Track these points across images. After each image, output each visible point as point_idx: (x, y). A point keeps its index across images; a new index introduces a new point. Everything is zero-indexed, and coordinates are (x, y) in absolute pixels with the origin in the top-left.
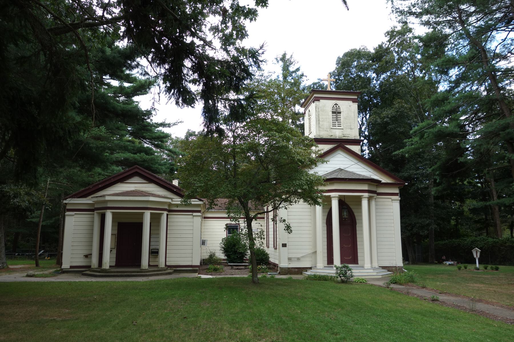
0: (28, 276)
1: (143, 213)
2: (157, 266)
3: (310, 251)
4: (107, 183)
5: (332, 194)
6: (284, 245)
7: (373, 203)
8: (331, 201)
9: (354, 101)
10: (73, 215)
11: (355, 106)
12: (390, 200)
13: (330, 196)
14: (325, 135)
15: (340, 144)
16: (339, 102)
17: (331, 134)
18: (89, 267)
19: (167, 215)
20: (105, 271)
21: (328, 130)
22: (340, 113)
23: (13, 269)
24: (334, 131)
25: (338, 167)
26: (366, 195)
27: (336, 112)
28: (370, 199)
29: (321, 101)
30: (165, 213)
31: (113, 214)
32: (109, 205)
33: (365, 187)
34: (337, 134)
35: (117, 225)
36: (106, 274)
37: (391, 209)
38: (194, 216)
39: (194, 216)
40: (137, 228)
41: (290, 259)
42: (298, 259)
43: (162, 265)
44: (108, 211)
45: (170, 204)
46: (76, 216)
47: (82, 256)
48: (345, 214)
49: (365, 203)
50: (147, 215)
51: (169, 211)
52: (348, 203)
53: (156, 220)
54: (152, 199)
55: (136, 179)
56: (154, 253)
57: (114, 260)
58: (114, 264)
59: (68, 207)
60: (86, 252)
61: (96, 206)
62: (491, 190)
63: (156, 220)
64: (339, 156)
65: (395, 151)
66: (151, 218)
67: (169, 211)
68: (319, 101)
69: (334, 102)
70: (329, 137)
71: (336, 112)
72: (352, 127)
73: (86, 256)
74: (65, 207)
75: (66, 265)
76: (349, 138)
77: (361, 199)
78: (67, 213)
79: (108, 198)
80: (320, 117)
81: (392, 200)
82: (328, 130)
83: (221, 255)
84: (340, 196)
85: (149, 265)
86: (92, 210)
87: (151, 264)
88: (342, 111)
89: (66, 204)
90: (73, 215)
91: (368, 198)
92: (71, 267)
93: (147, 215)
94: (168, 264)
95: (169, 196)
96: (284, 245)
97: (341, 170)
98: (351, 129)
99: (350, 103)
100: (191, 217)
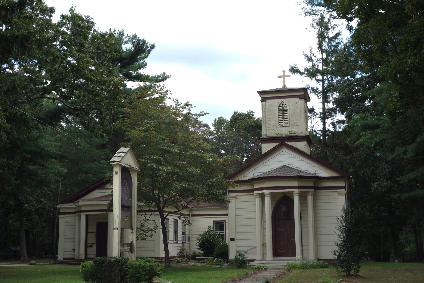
0: (31, 264)
5: (264, 192)
12: (336, 194)
13: (263, 193)
16: (284, 100)
17: (277, 132)
21: (275, 129)
22: (286, 110)
23: (225, 268)
24: (281, 129)
25: (283, 164)
27: (283, 111)
32: (83, 209)
33: (295, 183)
34: (284, 131)
35: (96, 224)
37: (335, 204)
44: (82, 213)
46: (66, 218)
59: (61, 211)
62: (139, 200)
64: (284, 153)
65: (355, 142)
68: (266, 101)
69: (280, 100)
70: (275, 136)
71: (283, 111)
72: (299, 123)
74: (59, 210)
75: (60, 257)
76: (295, 135)
78: (60, 216)
80: (267, 117)
81: (338, 193)
82: (275, 129)
83: (198, 251)
88: (288, 108)
89: (59, 208)
91: (298, 193)
92: (65, 259)
97: (284, 167)
98: (297, 125)
99: (297, 99)
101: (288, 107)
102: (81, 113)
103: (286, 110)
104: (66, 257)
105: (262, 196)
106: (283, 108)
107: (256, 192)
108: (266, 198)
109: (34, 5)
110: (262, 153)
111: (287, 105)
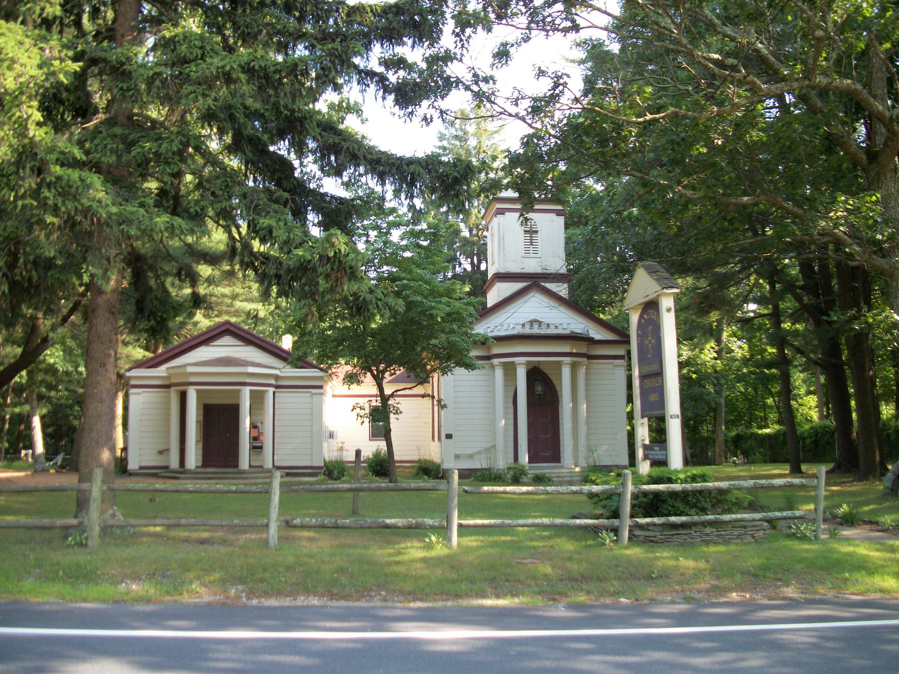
1: (264, 392)
2: (261, 467)
3: (484, 445)
4: (187, 346)
5: (516, 360)
6: (449, 436)
7: (582, 371)
8: (516, 369)
9: (559, 213)
10: (139, 394)
11: (561, 220)
12: (611, 366)
14: (515, 269)
15: (534, 282)
18: (166, 468)
19: (274, 393)
20: (191, 472)
22: (536, 232)
26: (567, 360)
28: (574, 367)
29: (507, 214)
30: (271, 390)
31: (198, 391)
32: (192, 379)
33: (566, 349)
34: (532, 266)
36: (194, 475)
38: (313, 394)
39: (615, 366)
40: (233, 411)
41: (457, 457)
42: (470, 456)
43: (269, 465)
45: (277, 377)
47: (155, 452)
48: (539, 389)
49: (566, 372)
50: (246, 391)
51: (277, 387)
52: (547, 371)
53: (257, 399)
54: (251, 370)
55: (227, 340)
56: (257, 447)
57: (200, 458)
58: (200, 464)
59: (133, 382)
60: (162, 448)
61: (174, 381)
63: (257, 399)
66: (251, 398)
67: (277, 387)
73: (161, 452)
77: (561, 366)
79: (190, 369)
81: (615, 366)
84: (528, 363)
85: (250, 466)
86: (168, 387)
87: (253, 464)
88: (539, 229)
90: (139, 394)
92: (141, 468)
93: (246, 391)
94: (276, 464)
95: (275, 365)
96: (449, 436)
99: (553, 216)
100: (308, 395)
101: (539, 226)
102: (119, 157)
103: (536, 232)
104: (319, 396)
105: (510, 370)
106: (531, 228)
107: (496, 361)
108: (518, 370)
109: (548, 570)
110: (489, 306)
111: (537, 223)
